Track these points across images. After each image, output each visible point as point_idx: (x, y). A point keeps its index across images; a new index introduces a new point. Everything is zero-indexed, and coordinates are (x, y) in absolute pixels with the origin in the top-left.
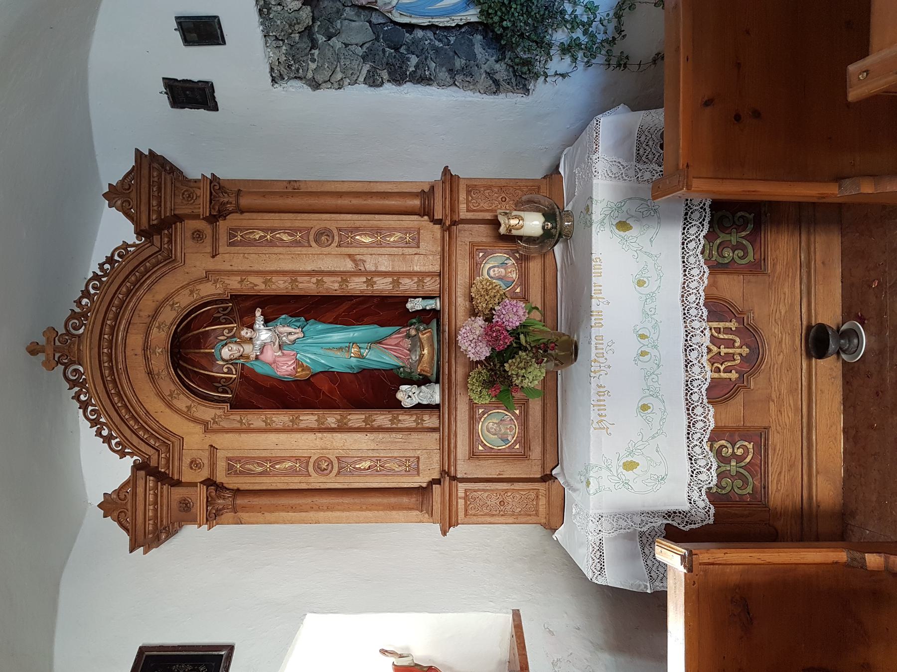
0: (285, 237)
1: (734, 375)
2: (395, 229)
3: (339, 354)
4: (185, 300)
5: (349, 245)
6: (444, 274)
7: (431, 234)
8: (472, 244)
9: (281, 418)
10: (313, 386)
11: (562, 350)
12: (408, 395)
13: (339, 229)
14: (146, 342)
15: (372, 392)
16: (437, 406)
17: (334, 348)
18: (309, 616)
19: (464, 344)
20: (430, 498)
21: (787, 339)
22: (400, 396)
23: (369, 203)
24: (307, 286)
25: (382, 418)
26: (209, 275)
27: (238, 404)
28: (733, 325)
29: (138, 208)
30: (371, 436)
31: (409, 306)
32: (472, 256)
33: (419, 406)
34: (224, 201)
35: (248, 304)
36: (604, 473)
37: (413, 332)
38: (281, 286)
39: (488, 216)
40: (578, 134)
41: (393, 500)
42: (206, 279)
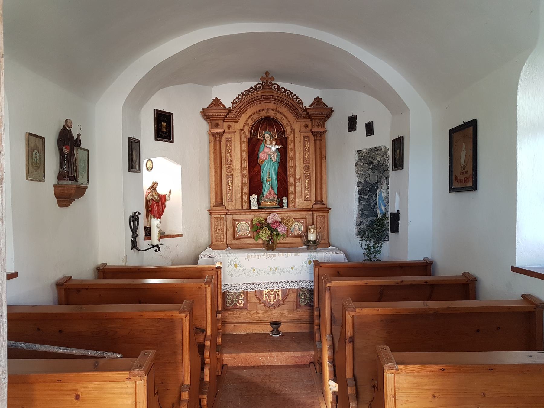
0: (307, 155)
1: (264, 299)
2: (310, 192)
3: (268, 174)
4: (285, 122)
5: (304, 177)
6: (296, 209)
7: (309, 205)
8: (306, 219)
9: (245, 155)
10: (256, 165)
11: (270, 246)
12: (254, 198)
13: (310, 173)
14: (270, 109)
15: (255, 186)
16: (250, 208)
17: (269, 173)
18: (180, 167)
19: (272, 215)
20: (218, 208)
21: (276, 315)
22: (254, 195)
23: (319, 183)
24: (290, 163)
25: (246, 189)
26: (293, 130)
27: (250, 140)
28: (280, 298)
29: (313, 109)
30: (240, 186)
31: (284, 198)
32: (302, 219)
33: (250, 202)
34: (319, 135)
35: (284, 142)
36: (233, 258)
37: (275, 199)
38: (290, 154)
39: (315, 223)
40: (340, 250)
41: (219, 193)
42: (292, 129)
